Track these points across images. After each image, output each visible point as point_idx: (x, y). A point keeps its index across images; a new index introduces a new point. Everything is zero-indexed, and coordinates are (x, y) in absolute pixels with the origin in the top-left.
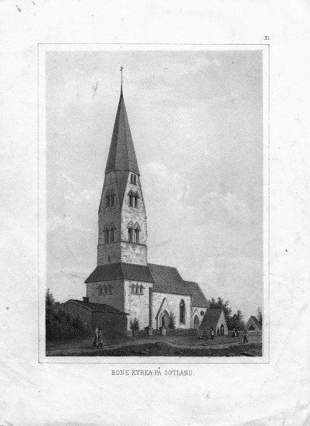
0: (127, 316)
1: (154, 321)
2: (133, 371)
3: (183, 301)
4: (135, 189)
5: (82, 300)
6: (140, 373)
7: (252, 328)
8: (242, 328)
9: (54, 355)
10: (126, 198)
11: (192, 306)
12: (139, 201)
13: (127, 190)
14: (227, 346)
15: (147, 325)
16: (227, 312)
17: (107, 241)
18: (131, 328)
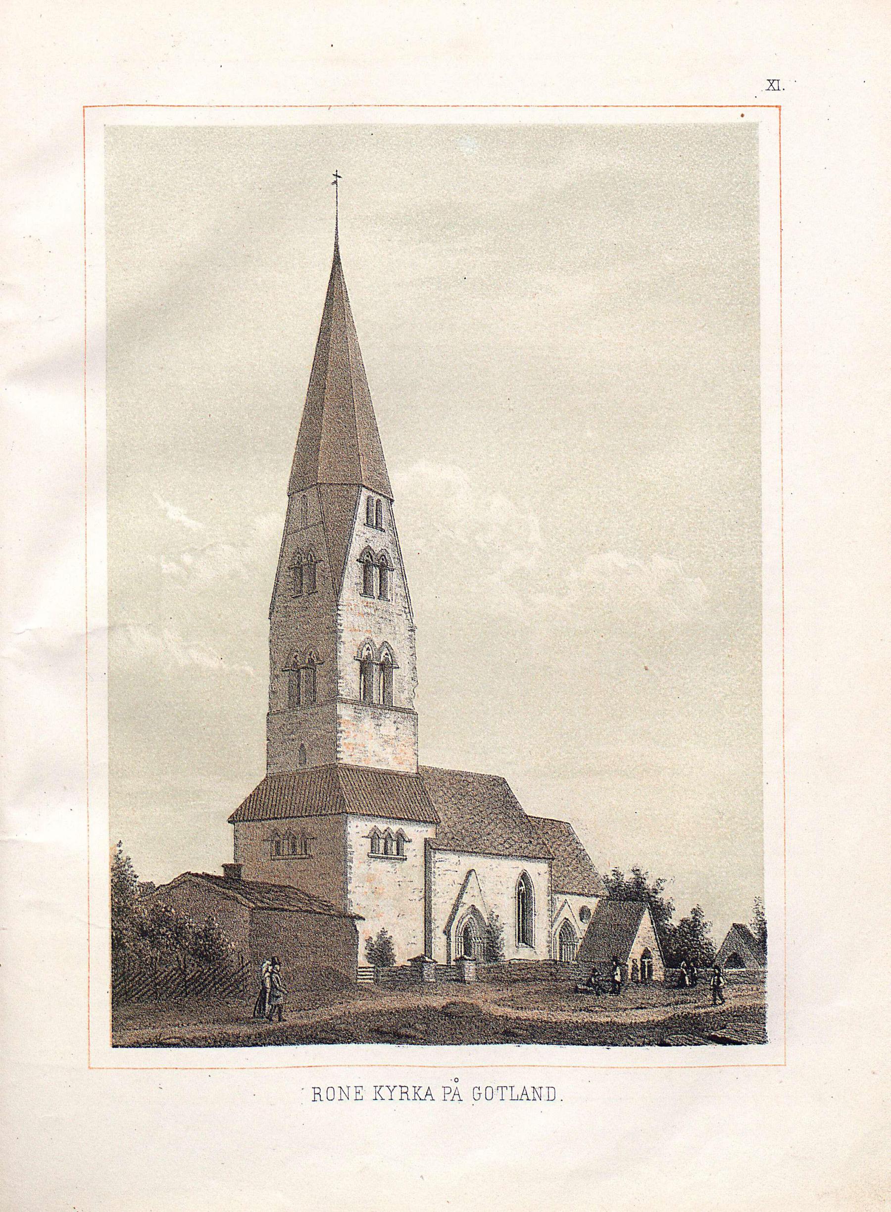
0: (358, 923)
1: (439, 941)
2: (378, 1089)
3: (524, 876)
4: (379, 543)
5: (221, 873)
6: (397, 1093)
7: (736, 960)
8: (708, 962)
9: (137, 1045)
10: (353, 572)
11: (555, 890)
12: (393, 579)
13: (356, 549)
14: (656, 1015)
15: (418, 950)
16: (659, 912)
17: (295, 702)
18: (369, 957)
